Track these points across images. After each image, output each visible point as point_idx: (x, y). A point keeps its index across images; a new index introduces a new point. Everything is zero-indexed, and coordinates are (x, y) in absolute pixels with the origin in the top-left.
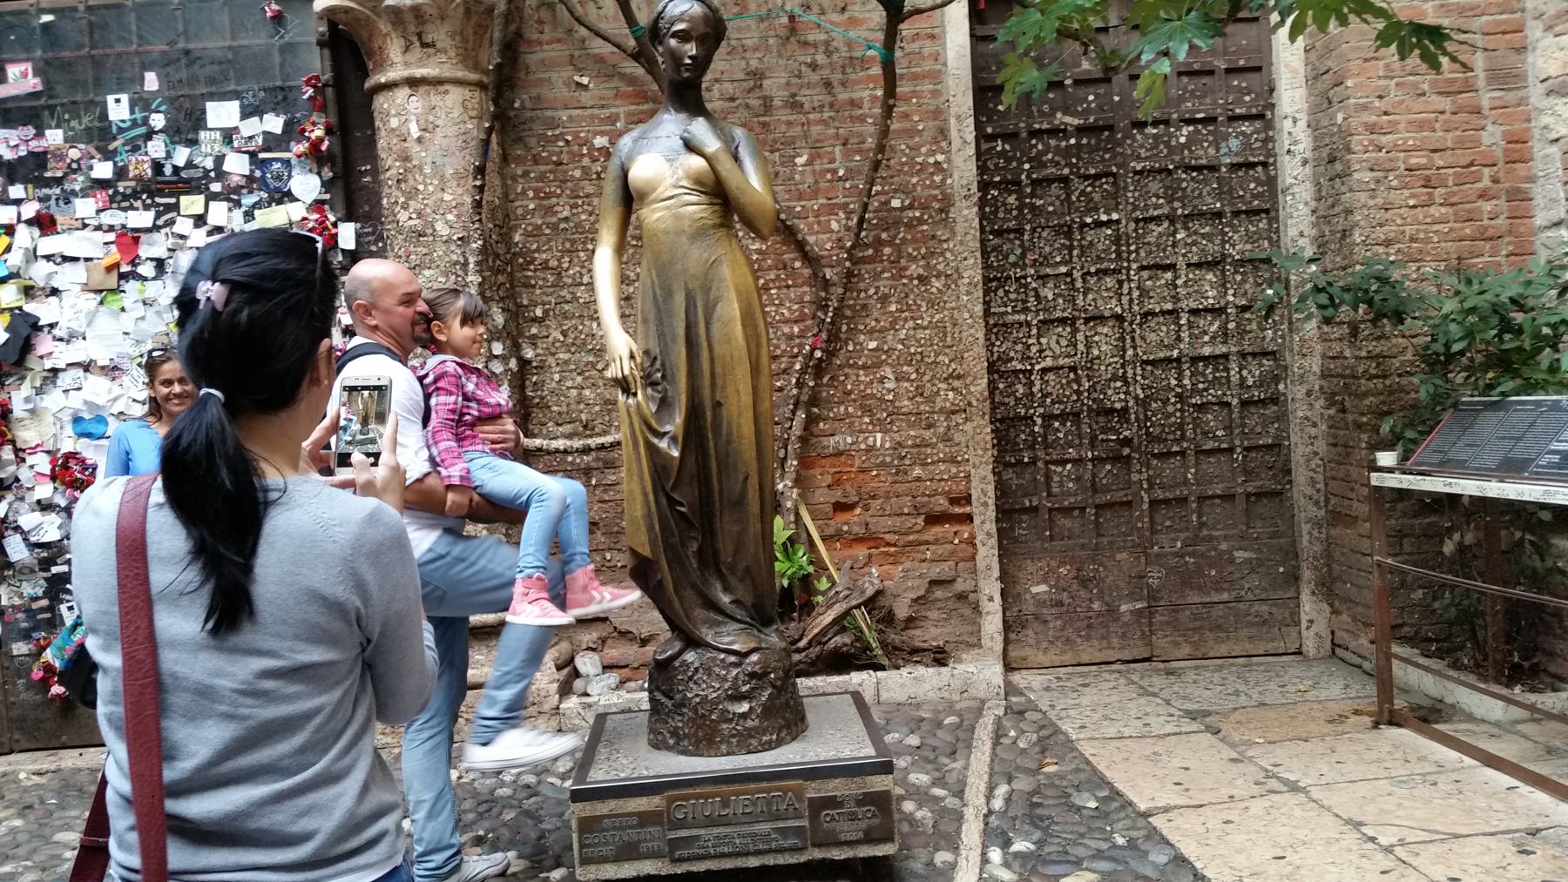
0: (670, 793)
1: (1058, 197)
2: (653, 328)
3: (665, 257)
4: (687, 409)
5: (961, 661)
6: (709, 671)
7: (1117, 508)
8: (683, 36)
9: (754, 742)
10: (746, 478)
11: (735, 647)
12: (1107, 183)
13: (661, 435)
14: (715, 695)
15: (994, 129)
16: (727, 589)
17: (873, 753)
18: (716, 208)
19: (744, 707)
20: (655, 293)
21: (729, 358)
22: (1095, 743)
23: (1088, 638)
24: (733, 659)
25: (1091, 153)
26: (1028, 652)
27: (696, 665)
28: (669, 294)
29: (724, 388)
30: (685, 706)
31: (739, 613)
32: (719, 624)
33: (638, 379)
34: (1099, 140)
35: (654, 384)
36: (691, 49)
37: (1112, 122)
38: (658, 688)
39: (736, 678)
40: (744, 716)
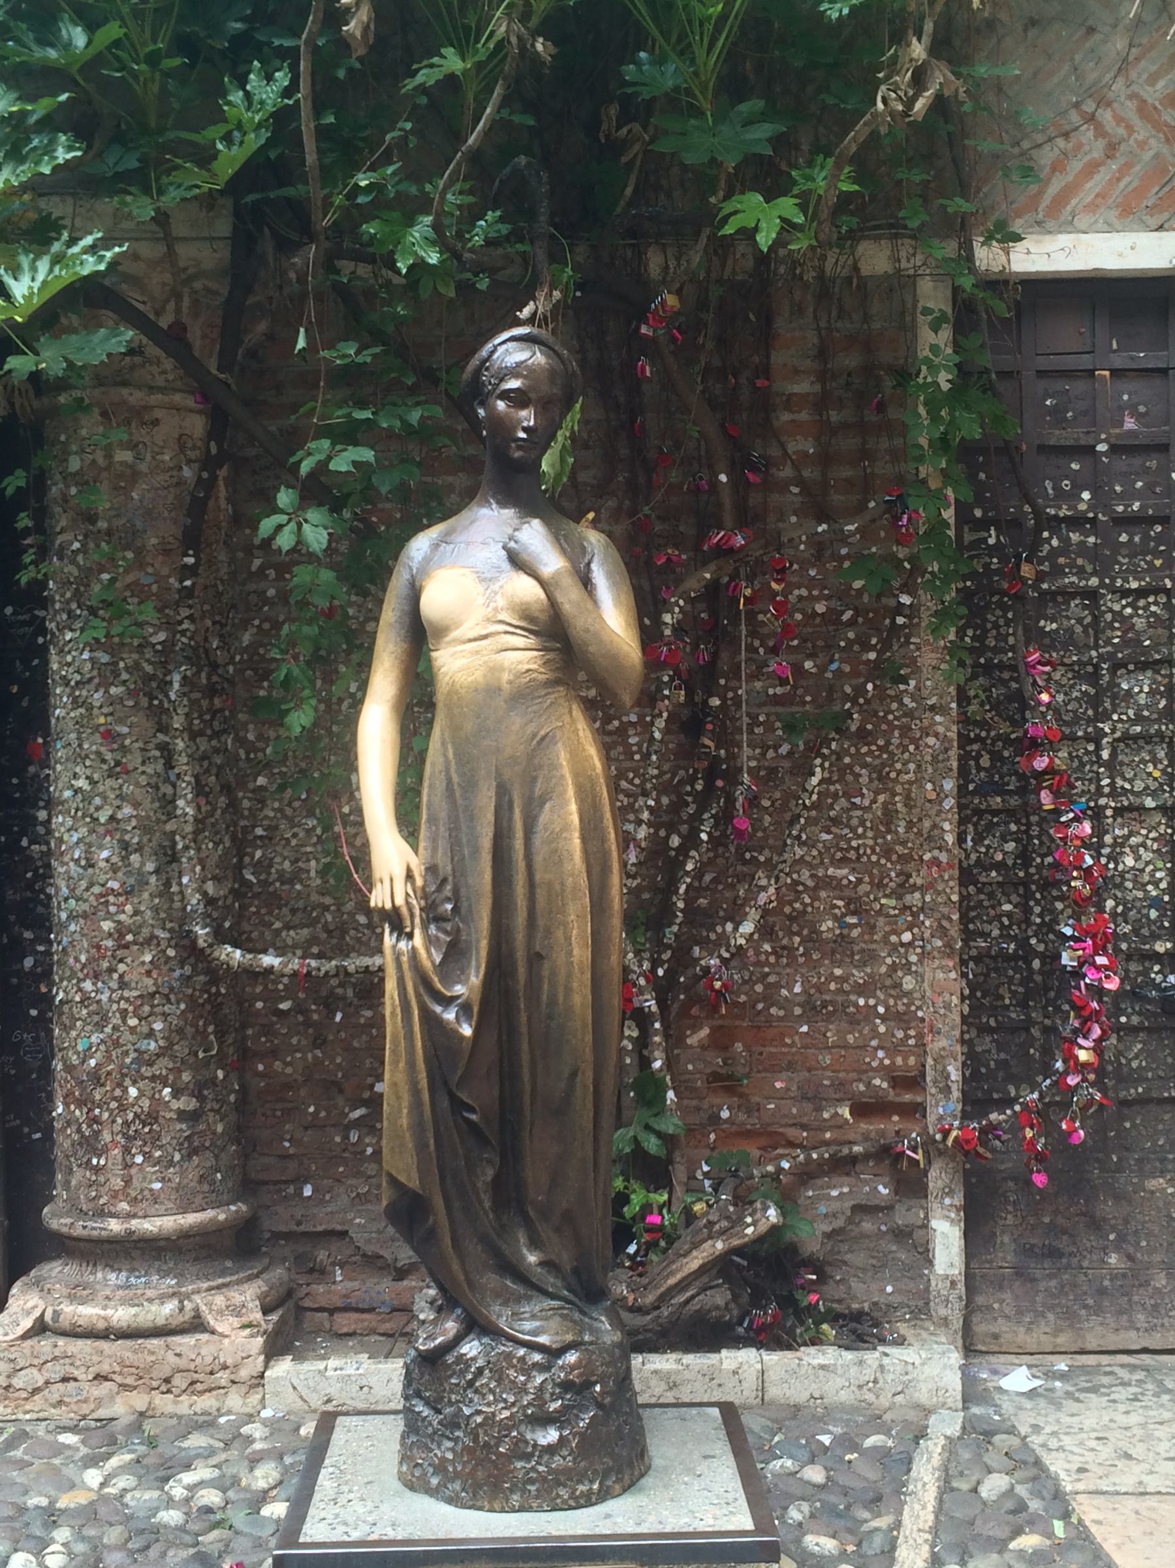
0: (439, 986)
1: (1080, 621)
2: (443, 831)
3: (469, 726)
4: (488, 962)
5: (901, 1342)
6: (500, 1377)
7: (1151, 1107)
8: (518, 399)
9: (564, 1492)
10: (574, 1074)
11: (543, 1339)
12: (1156, 603)
13: (447, 1002)
14: (506, 1414)
15: (985, 513)
16: (535, 1243)
17: (749, 1525)
18: (551, 656)
19: (551, 1436)
20: (449, 781)
21: (558, 887)
22: (1099, 1500)
23: (1098, 1310)
24: (537, 1357)
25: (1133, 556)
26: (1001, 1326)
27: (480, 1363)
28: (470, 785)
29: (548, 932)
30: (458, 1427)
31: (551, 1282)
32: (519, 1300)
33: (417, 912)
34: (1146, 538)
35: (439, 919)
36: (528, 417)
37: (1165, 441)
38: (418, 1394)
39: (541, 1388)
40: (551, 1450)
